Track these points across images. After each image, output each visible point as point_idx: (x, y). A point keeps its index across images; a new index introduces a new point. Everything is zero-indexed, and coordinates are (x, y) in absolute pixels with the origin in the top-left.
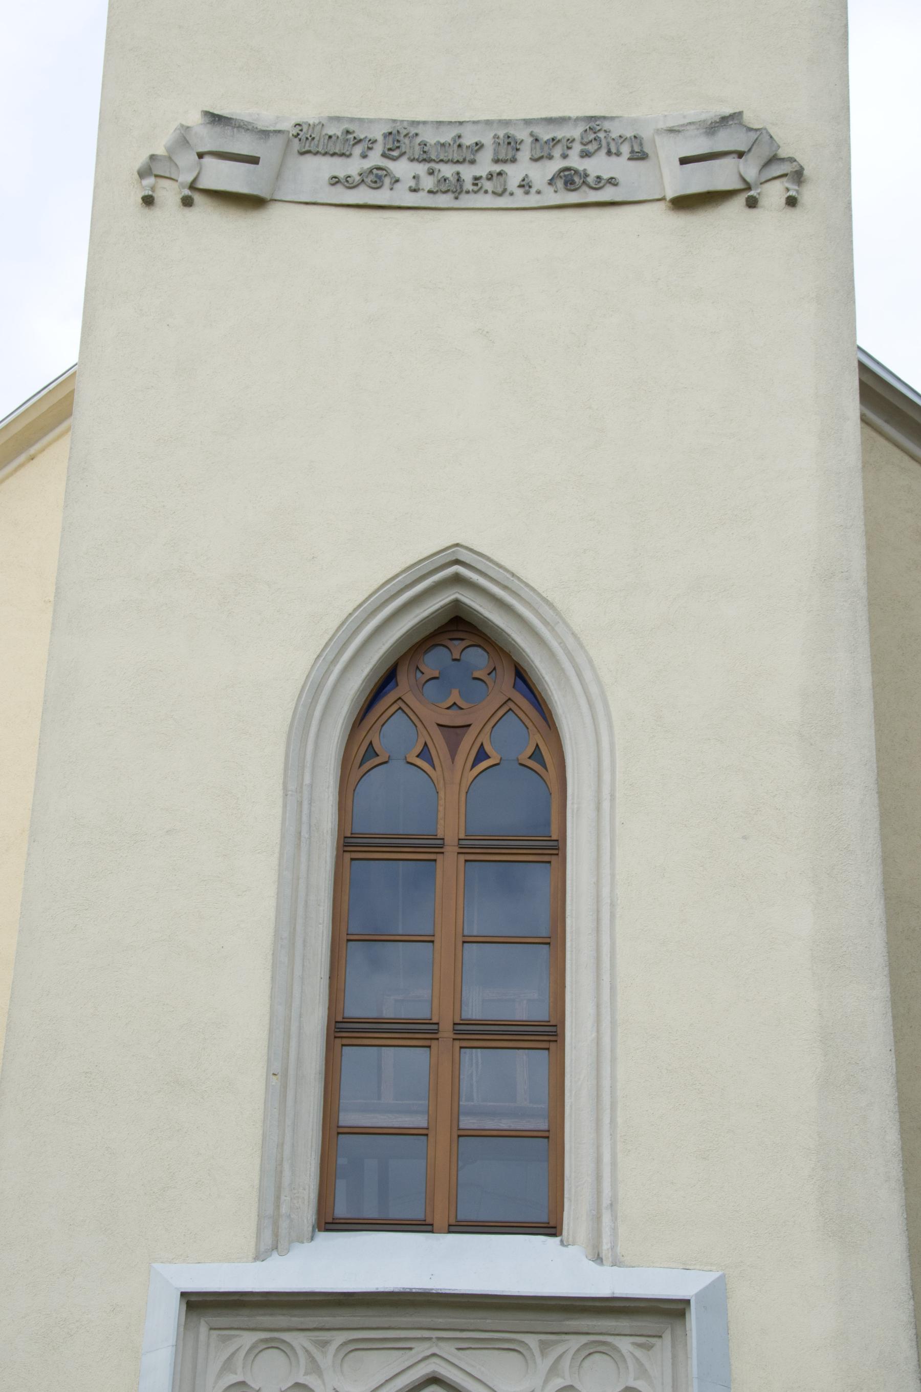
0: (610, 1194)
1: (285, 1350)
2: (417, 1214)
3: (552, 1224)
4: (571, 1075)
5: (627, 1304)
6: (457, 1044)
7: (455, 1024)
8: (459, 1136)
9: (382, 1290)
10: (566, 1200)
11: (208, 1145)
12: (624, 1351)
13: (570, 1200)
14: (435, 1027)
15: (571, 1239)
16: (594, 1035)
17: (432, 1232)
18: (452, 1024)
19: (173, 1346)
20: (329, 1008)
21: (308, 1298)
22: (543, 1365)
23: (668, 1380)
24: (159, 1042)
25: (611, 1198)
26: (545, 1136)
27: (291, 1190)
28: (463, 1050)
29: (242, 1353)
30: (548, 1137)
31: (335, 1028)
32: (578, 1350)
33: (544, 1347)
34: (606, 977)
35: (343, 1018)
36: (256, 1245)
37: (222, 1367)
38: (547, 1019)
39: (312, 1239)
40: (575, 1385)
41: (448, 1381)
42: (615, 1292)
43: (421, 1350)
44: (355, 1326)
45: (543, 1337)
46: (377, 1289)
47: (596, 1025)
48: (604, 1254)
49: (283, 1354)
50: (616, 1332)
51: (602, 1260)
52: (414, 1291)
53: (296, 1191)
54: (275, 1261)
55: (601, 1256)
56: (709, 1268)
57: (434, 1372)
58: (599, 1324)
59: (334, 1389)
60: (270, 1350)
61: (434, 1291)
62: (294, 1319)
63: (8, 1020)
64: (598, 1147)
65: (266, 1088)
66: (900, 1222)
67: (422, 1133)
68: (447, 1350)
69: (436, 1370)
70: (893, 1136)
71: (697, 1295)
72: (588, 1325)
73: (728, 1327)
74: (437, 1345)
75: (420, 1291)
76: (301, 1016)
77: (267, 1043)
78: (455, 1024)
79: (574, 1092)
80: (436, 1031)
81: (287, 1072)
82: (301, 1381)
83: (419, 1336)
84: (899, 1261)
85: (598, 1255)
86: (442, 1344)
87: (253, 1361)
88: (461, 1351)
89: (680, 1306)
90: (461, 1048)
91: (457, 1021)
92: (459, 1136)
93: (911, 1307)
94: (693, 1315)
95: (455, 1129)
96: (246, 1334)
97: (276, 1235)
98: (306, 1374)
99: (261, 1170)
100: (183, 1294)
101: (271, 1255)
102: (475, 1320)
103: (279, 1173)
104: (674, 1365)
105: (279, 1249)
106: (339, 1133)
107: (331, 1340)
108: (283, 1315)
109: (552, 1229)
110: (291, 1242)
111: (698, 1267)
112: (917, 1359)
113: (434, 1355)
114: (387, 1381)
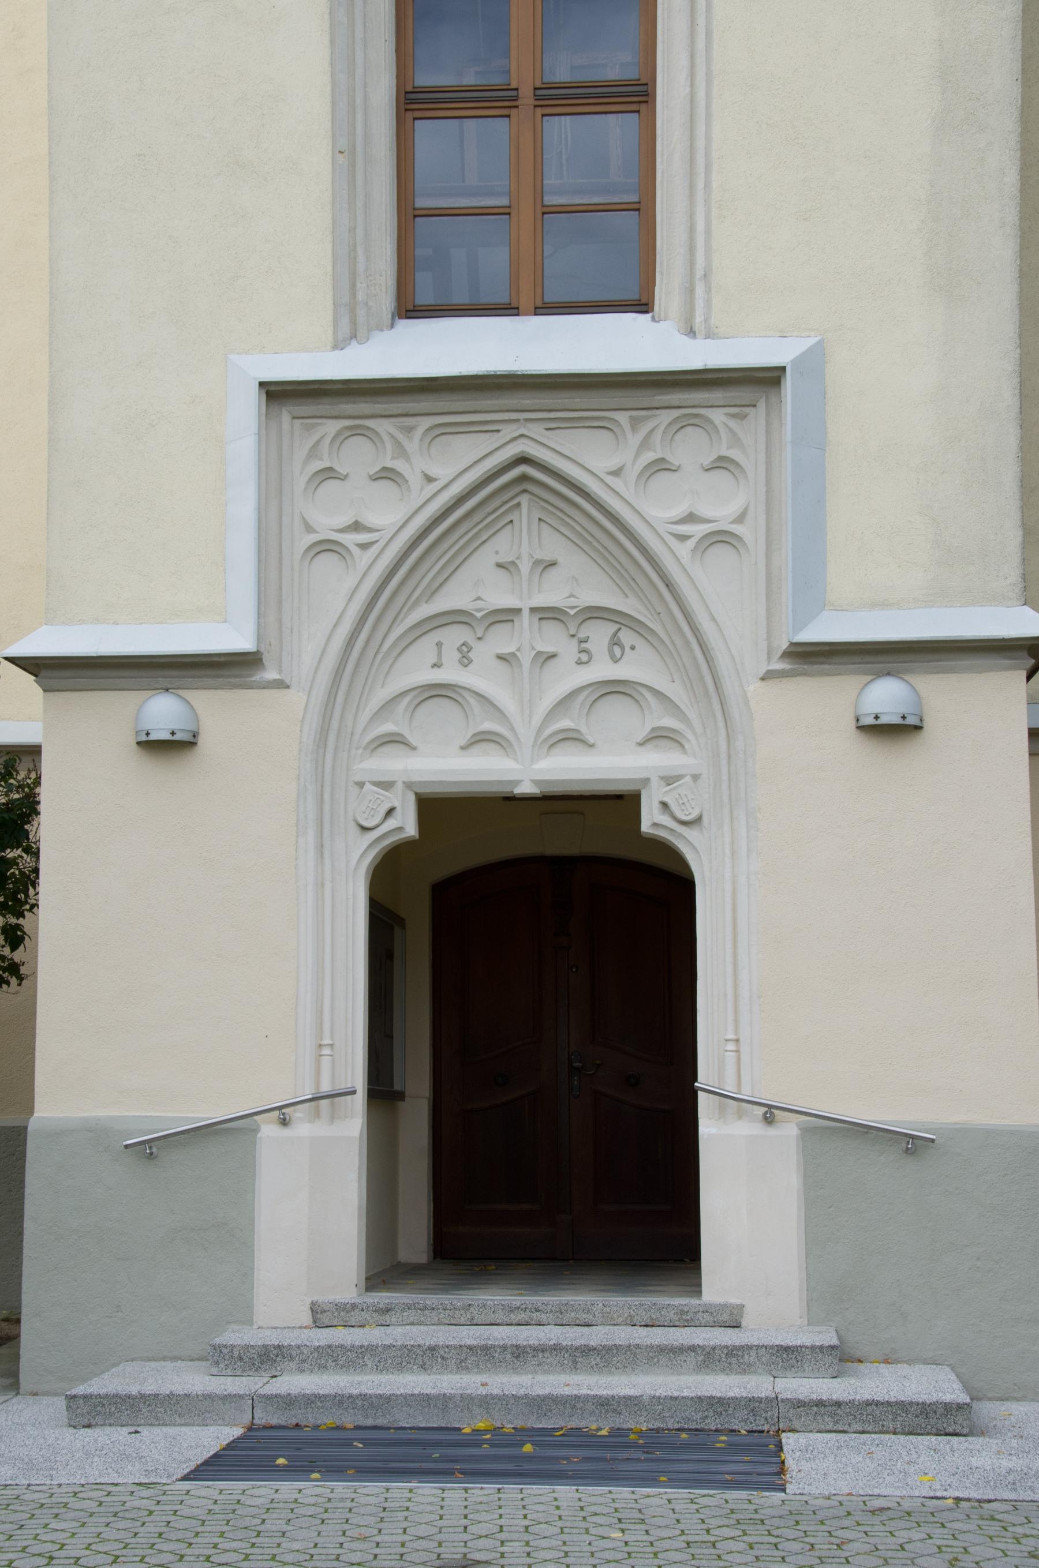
0: (704, 265)
1: (371, 436)
2: (503, 298)
3: (643, 301)
4: (663, 139)
5: (719, 375)
6: (539, 111)
7: (535, 89)
8: (544, 213)
9: (466, 374)
10: (657, 274)
11: (275, 230)
12: (717, 422)
13: (662, 274)
14: (514, 93)
15: (662, 315)
16: (688, 90)
17: (518, 315)
18: (533, 89)
19: (255, 434)
20: (398, 77)
21: (390, 385)
22: (634, 440)
23: (762, 447)
24: (214, 119)
25: (705, 268)
26: (635, 208)
27: (367, 277)
28: (545, 118)
29: (327, 441)
30: (638, 210)
31: (405, 99)
32: (670, 424)
33: (635, 423)
34: (701, 21)
35: (414, 88)
36: (334, 334)
37: (307, 455)
38: (637, 77)
39: (392, 326)
40: (668, 458)
41: (538, 461)
42: (708, 364)
43: (509, 432)
44: (441, 411)
45: (634, 413)
46: (461, 373)
47: (690, 78)
48: (697, 325)
49: (368, 441)
50: (709, 404)
51: (695, 333)
52: (498, 373)
53: (372, 278)
54: (354, 350)
55: (694, 329)
56: (807, 334)
57: (523, 452)
58: (691, 396)
59: (423, 472)
60: (355, 438)
61: (519, 373)
62: (377, 406)
63: (49, 96)
64: (692, 216)
65: (333, 167)
66: (1013, 270)
67: (505, 212)
68: (536, 431)
69: (524, 450)
70: (1012, 178)
71: (792, 361)
72: (679, 399)
73: (825, 392)
74: (525, 426)
75: (504, 373)
76: (365, 86)
77: (330, 117)
78: (535, 89)
79: (665, 157)
80: (515, 98)
81: (355, 150)
82: (389, 465)
83: (507, 418)
84: (1009, 311)
85: (691, 328)
86: (529, 425)
87: (339, 448)
88: (550, 431)
89: (775, 374)
90: (543, 115)
91: (538, 85)
92: (544, 213)
93: (1017, 356)
94: (788, 382)
95: (539, 206)
96: (330, 422)
97: (354, 323)
98: (393, 458)
99: (333, 256)
100: (262, 384)
101: (350, 344)
102: (563, 400)
103: (353, 260)
104: (768, 432)
105: (358, 338)
106: (415, 216)
107: (416, 426)
108: (366, 402)
109: (643, 305)
110: (369, 330)
111: (796, 333)
112: (1019, 407)
113: (522, 436)
114: (475, 462)
